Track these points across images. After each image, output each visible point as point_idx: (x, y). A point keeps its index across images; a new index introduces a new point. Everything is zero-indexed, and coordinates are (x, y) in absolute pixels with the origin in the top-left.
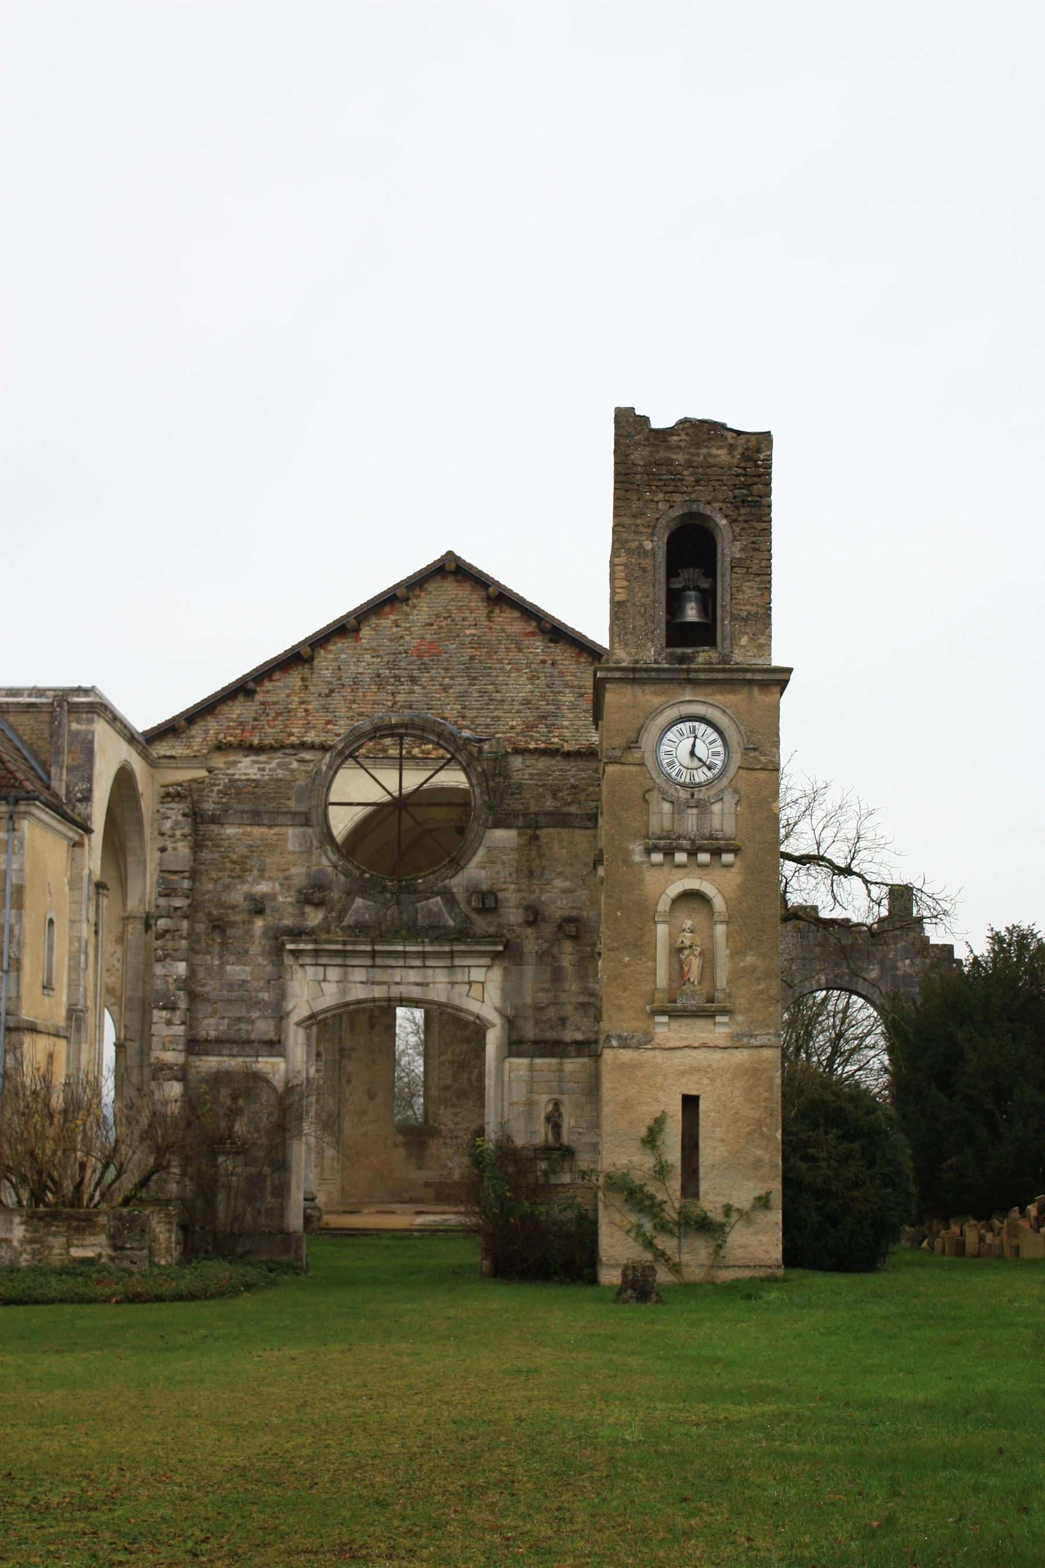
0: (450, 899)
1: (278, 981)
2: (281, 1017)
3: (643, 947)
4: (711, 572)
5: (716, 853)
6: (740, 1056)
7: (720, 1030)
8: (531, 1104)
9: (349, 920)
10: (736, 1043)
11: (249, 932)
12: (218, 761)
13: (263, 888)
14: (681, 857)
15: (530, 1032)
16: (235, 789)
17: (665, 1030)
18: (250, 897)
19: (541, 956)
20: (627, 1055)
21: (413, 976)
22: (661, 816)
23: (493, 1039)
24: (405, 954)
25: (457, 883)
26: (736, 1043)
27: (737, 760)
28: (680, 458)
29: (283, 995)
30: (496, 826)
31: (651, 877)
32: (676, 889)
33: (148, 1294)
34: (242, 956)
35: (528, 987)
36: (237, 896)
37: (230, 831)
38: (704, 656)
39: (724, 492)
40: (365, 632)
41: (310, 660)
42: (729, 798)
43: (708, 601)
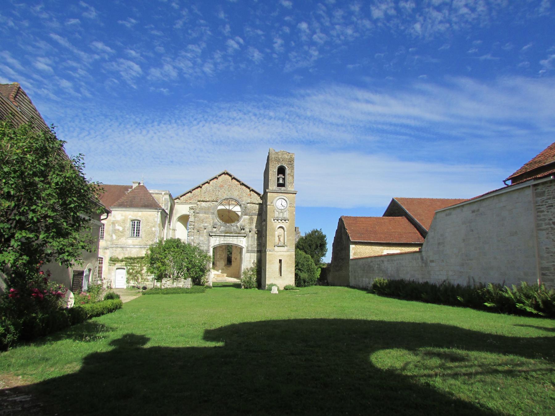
0: (237, 227)
1: (209, 241)
2: (209, 246)
3: (273, 235)
4: (284, 175)
5: (285, 220)
6: (288, 253)
7: (285, 249)
8: (250, 261)
9: (220, 230)
10: (288, 251)
11: (203, 233)
12: (199, 203)
13: (206, 225)
14: (279, 221)
15: (250, 249)
16: (202, 209)
17: (277, 249)
18: (204, 226)
19: (252, 237)
20: (270, 253)
21: (231, 239)
22: (276, 214)
23: (244, 251)
24: (230, 236)
25: (238, 224)
26: (288, 251)
27: (288, 205)
28: (280, 157)
29: (209, 242)
30: (245, 215)
31: (275, 224)
32: (278, 226)
33: (93, 311)
34: (202, 236)
35: (250, 241)
36: (202, 225)
37: (201, 215)
38: (283, 188)
39: (287, 163)
40: (211, 182)
41: (201, 187)
42: (287, 211)
43: (284, 179)
